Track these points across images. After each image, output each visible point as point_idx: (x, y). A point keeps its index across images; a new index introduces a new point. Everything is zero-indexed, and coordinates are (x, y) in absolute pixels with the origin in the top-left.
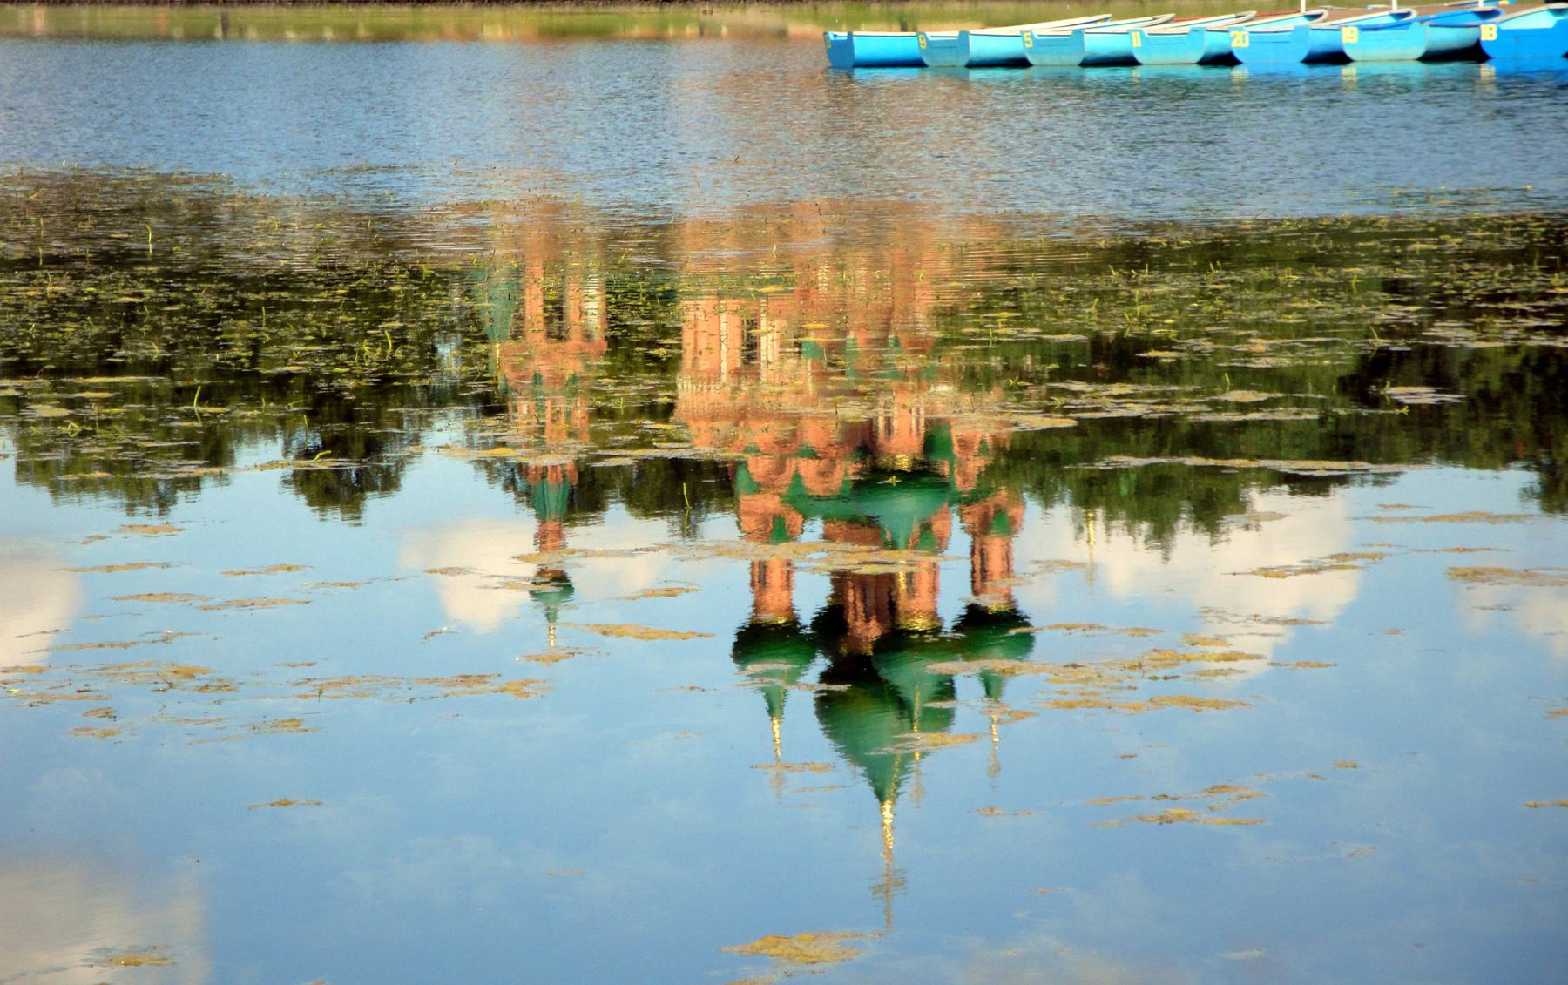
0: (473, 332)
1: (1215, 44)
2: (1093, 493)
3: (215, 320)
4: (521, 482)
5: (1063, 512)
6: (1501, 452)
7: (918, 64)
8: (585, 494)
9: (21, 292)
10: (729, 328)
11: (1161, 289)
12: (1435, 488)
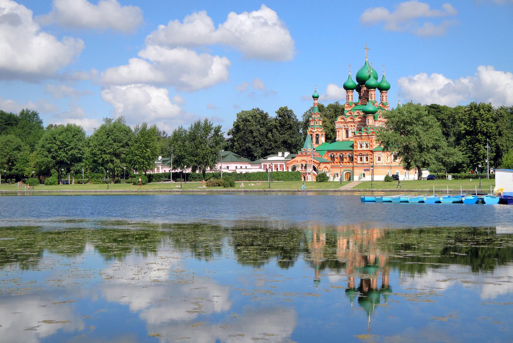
0: (306, 241)
1: (421, 199)
2: (402, 268)
3: (268, 238)
4: (312, 264)
5: (397, 271)
6: (466, 263)
7: (375, 201)
8: (323, 266)
9: (241, 234)
10: (345, 241)
11: (414, 236)
12: (454, 268)
